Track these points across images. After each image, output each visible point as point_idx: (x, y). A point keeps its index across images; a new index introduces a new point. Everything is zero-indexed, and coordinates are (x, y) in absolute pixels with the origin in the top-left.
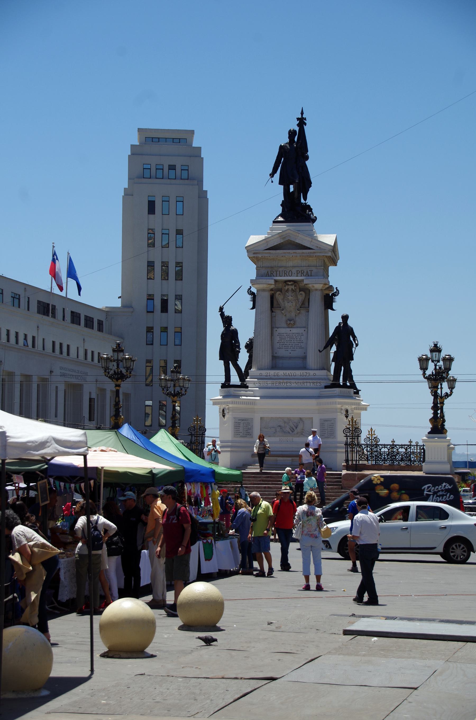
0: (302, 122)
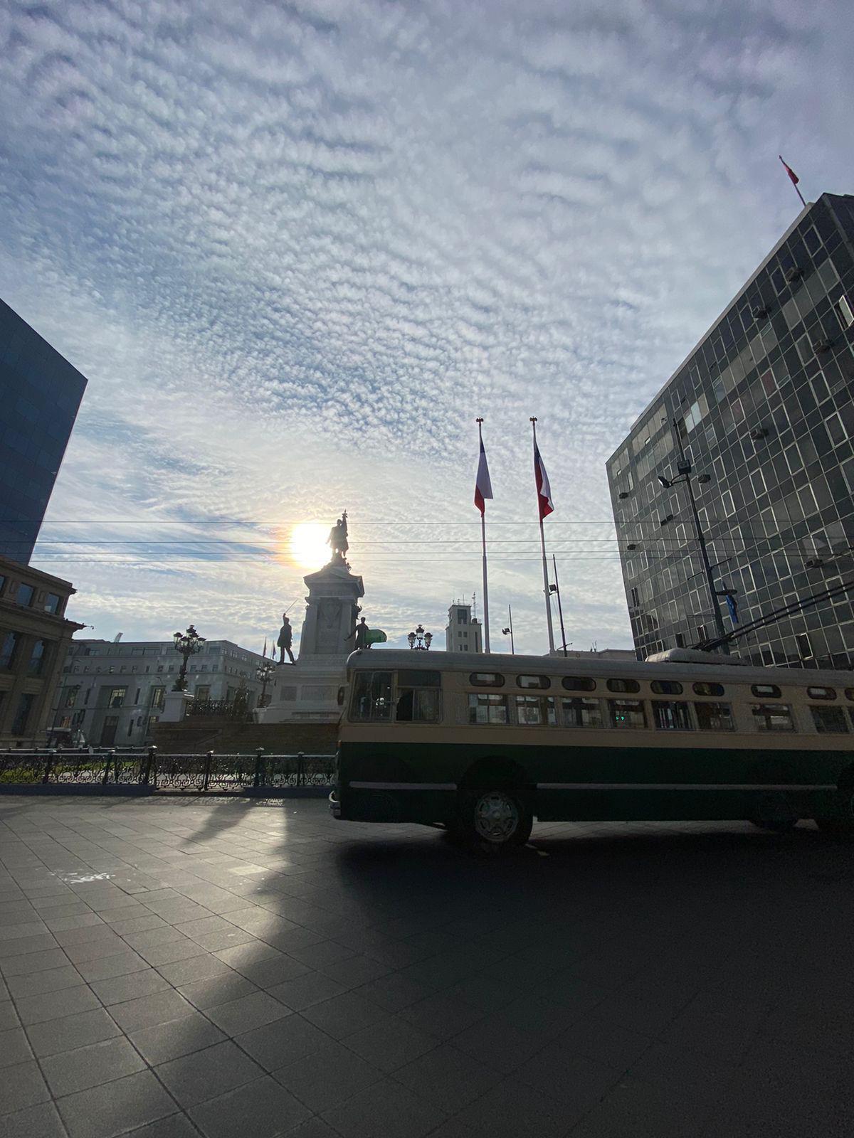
0: (345, 516)
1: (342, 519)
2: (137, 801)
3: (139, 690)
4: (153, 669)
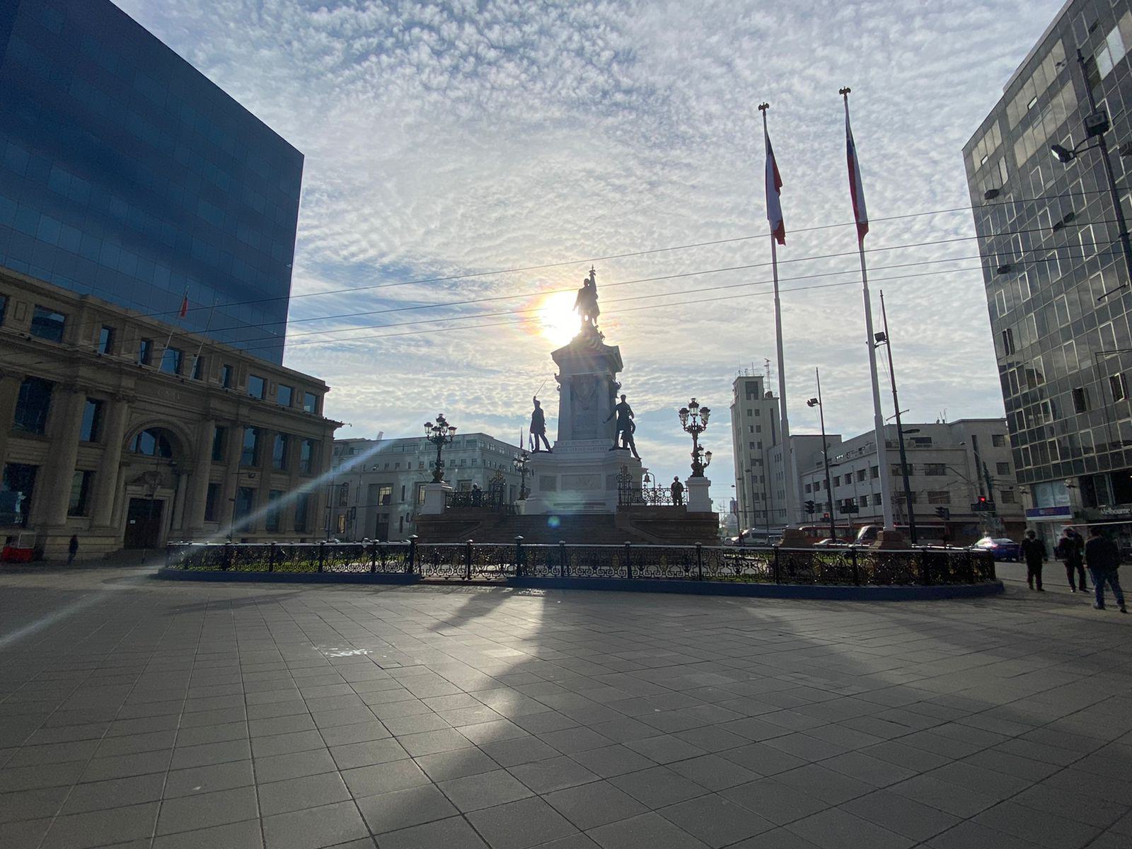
0: (592, 273)
1: (589, 278)
2: (402, 588)
3: (404, 487)
4: (415, 467)
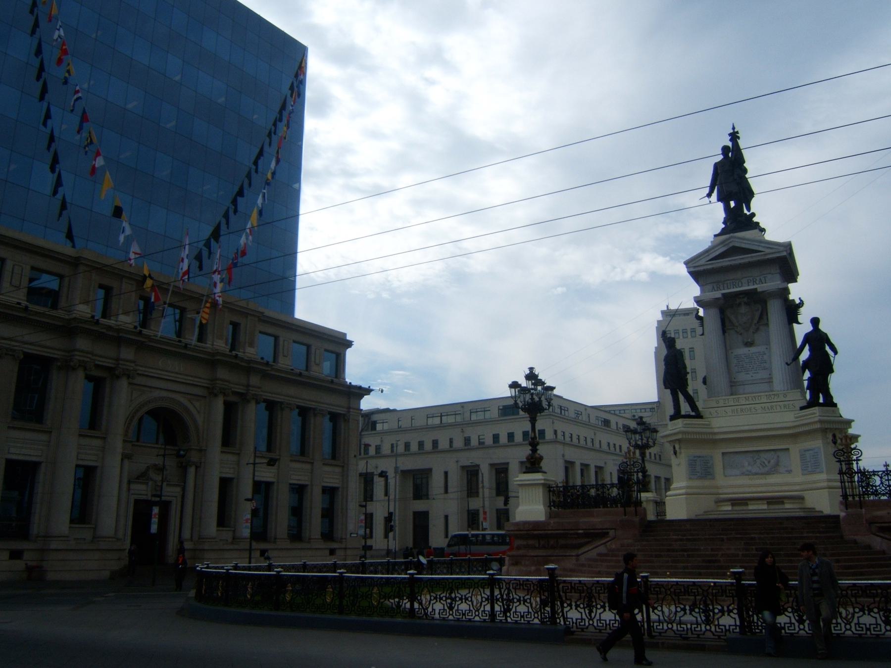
0: (734, 136)
1: (730, 144)
